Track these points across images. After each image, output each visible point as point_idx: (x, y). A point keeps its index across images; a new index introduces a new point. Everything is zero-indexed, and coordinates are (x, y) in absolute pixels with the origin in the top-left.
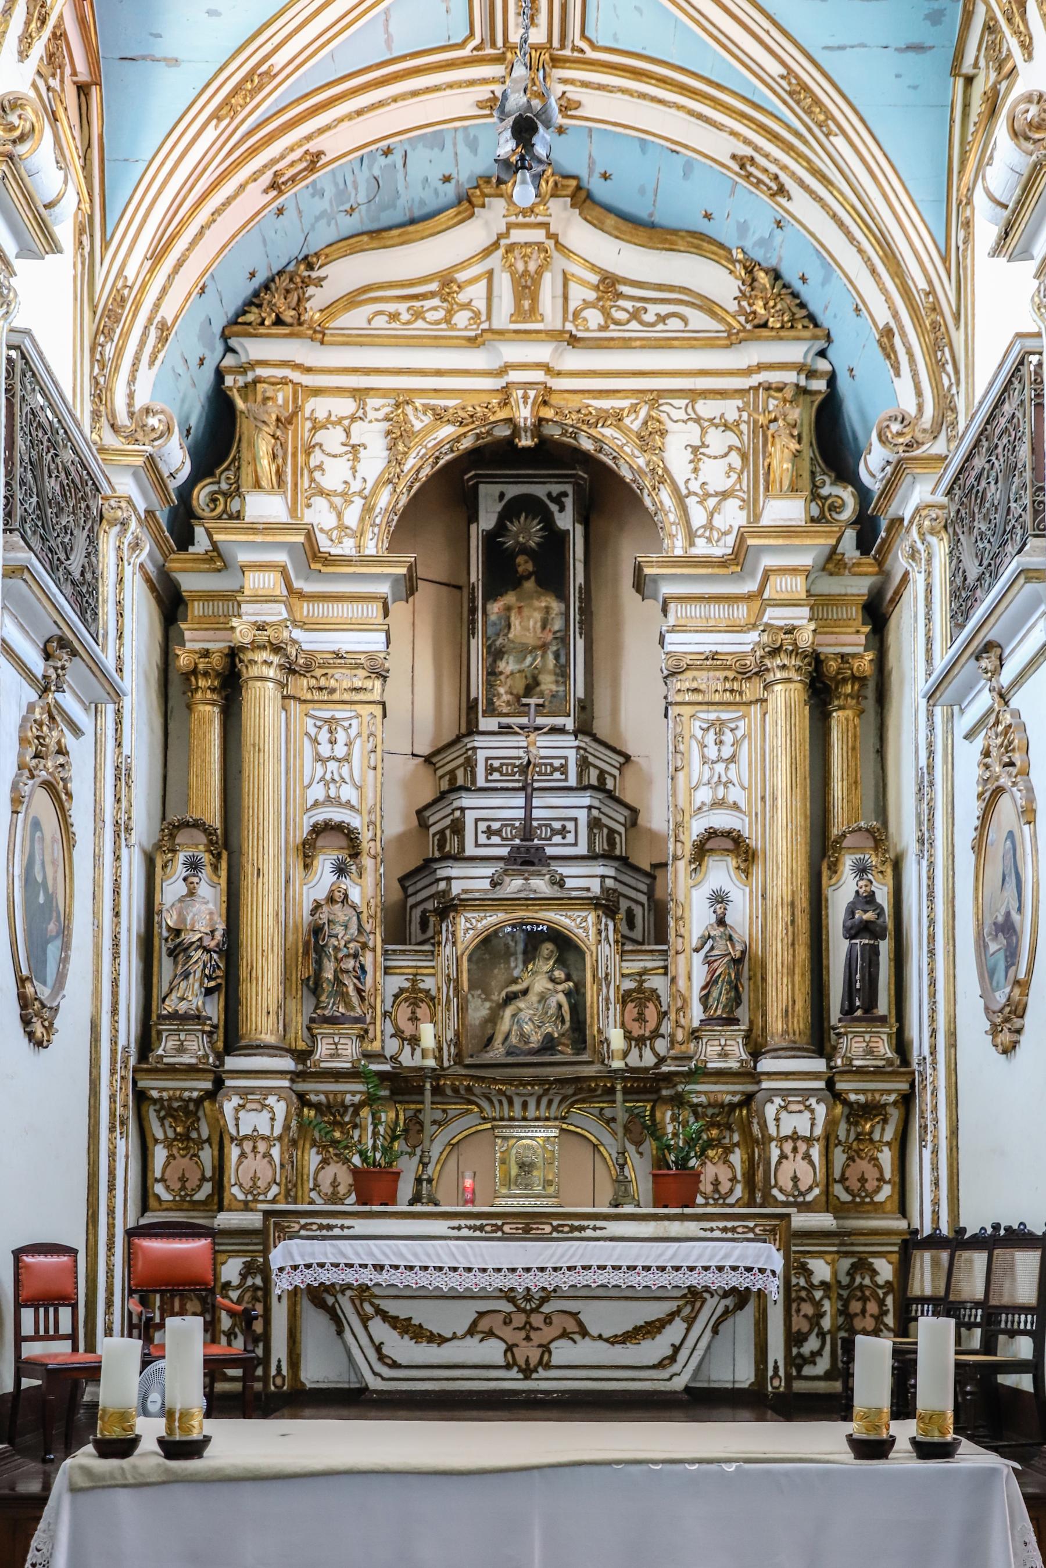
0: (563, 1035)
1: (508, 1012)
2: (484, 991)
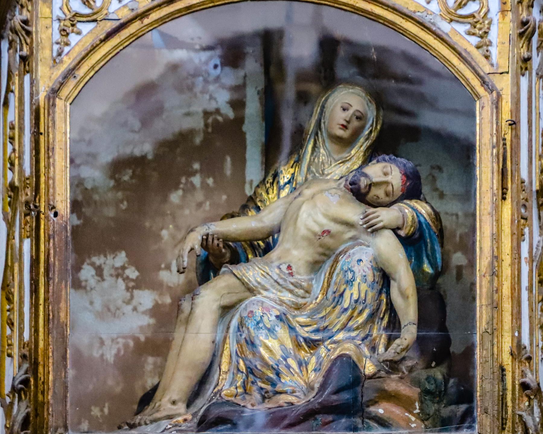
0: (393, 366)
1: (210, 297)
2: (135, 260)
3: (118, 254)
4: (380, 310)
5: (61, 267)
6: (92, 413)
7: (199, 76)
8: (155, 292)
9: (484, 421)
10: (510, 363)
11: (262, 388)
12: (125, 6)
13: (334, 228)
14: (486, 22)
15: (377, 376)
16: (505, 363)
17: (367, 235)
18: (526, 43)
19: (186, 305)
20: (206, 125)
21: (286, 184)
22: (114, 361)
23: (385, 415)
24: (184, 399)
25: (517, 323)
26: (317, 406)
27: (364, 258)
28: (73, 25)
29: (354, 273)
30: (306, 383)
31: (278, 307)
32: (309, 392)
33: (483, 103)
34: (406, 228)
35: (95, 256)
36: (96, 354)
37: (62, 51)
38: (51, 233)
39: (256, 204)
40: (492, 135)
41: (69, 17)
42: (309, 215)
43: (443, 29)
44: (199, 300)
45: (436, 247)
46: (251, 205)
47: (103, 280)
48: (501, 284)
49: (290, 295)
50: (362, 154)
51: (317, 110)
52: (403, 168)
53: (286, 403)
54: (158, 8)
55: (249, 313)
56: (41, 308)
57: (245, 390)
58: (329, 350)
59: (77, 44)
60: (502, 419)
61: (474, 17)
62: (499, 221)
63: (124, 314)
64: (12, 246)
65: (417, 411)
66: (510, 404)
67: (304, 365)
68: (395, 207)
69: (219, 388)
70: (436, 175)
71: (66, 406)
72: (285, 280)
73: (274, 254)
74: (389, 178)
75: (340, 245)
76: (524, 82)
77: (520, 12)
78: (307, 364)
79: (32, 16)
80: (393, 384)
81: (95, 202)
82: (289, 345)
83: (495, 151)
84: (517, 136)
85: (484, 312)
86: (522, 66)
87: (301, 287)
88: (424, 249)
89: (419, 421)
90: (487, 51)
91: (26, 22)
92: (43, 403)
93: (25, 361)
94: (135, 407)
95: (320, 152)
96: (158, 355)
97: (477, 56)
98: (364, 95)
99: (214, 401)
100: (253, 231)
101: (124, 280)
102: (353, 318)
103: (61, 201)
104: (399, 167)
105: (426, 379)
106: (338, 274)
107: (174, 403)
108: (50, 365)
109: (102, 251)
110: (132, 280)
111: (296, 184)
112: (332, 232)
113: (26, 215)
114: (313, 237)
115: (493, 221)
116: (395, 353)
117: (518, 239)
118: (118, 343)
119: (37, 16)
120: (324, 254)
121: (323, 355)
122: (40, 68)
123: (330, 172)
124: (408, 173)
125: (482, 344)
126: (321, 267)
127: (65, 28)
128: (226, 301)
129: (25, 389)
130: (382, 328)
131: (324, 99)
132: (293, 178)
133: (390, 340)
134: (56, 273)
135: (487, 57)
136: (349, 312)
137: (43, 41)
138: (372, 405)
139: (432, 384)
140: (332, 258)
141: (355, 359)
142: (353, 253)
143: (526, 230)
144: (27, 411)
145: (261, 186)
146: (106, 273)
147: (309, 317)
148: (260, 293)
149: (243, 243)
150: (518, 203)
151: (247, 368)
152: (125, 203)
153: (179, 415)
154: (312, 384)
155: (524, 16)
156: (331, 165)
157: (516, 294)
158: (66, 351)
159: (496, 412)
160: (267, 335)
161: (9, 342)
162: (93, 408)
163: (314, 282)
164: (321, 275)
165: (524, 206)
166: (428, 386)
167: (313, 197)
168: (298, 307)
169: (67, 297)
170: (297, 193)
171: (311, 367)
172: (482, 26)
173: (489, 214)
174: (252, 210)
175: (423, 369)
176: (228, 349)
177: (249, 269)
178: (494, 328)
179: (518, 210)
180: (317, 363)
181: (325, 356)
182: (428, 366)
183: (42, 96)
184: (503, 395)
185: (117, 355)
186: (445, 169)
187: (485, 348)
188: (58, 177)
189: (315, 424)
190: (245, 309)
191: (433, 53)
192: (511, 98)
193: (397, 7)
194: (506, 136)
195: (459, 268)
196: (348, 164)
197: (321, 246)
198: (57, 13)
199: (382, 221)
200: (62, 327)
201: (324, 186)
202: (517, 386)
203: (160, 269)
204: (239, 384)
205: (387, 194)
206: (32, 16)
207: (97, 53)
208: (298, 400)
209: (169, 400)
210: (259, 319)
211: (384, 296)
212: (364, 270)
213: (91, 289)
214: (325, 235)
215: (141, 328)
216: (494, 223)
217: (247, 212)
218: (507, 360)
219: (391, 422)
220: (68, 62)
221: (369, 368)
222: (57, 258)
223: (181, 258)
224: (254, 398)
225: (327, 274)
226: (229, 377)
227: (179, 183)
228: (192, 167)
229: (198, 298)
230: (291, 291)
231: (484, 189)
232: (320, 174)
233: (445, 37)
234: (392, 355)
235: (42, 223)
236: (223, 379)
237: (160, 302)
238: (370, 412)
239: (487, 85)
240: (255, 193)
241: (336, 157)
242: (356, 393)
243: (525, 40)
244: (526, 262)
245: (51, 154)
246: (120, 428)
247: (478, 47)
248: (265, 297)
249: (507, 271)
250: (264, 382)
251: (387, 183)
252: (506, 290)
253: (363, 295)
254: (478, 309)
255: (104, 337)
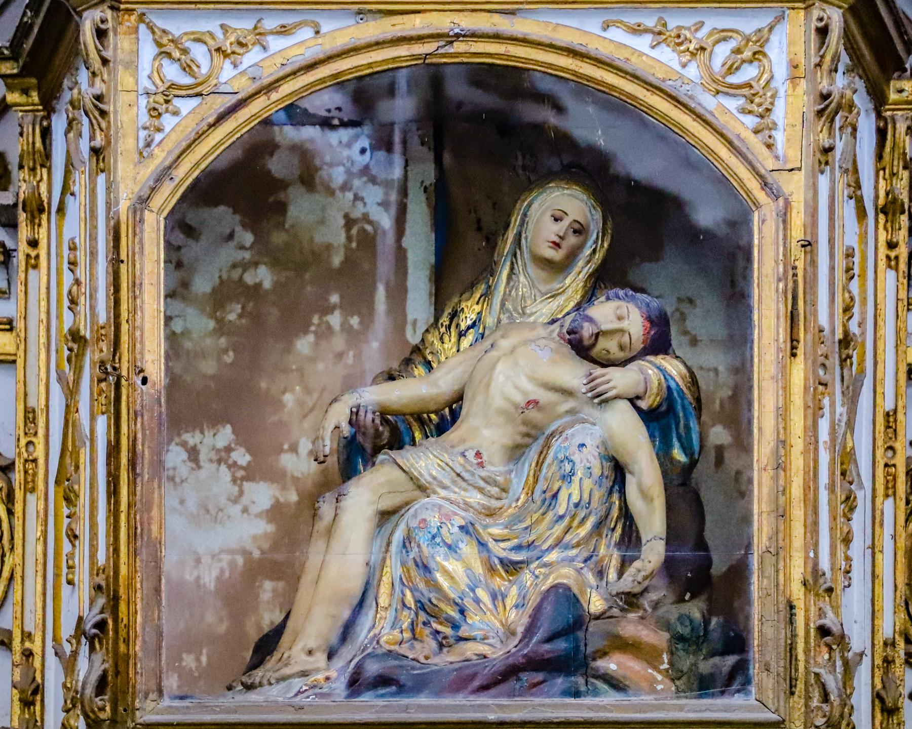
0: (630, 600)
2: (244, 437)
3: (221, 429)
4: (610, 517)
5: (152, 457)
6: (184, 664)
7: (338, 165)
8: (275, 485)
9: (764, 682)
10: (802, 597)
11: (438, 632)
12: (243, 73)
13: (545, 397)
14: (769, 94)
15: (608, 614)
16: (794, 597)
17: (593, 407)
18: (827, 125)
19: (326, 508)
20: (349, 238)
21: (469, 328)
22: (215, 587)
23: (619, 671)
24: (324, 647)
25: (812, 538)
26: (522, 660)
27: (588, 442)
28: (167, 102)
29: (574, 464)
30: (503, 625)
31: (463, 513)
32: (507, 638)
33: (765, 215)
34: (649, 397)
35: (187, 432)
36: (189, 577)
37: (152, 141)
38: (138, 408)
39: (425, 358)
40: (776, 262)
41: (161, 89)
42: (508, 378)
43: (705, 104)
44: (347, 503)
45: (691, 424)
46: (418, 359)
47: (199, 467)
48: (788, 482)
49: (479, 496)
50: (582, 284)
51: (516, 220)
52: (645, 309)
53: (476, 655)
54: (292, 77)
55: (420, 523)
56: (123, 517)
57: (414, 635)
58: (537, 577)
59: (173, 129)
60: (791, 679)
61: (751, 87)
62: (786, 389)
63: (229, 517)
64: (74, 422)
65: (666, 666)
66: (801, 656)
67: (500, 598)
68: (633, 366)
69: (376, 631)
70: (686, 311)
71: (160, 661)
72: (473, 474)
73: (452, 435)
74: (624, 325)
75: (552, 422)
76: (824, 181)
77: (819, 80)
78: (504, 597)
79: (108, 89)
80: (631, 627)
81: (188, 352)
82: (479, 569)
83: (781, 285)
84: (813, 263)
85: (765, 522)
86: (822, 160)
87: (496, 484)
88: (673, 426)
89: (667, 681)
90: (770, 137)
91: (99, 98)
92: (128, 655)
93: (100, 594)
94: (248, 655)
95: (519, 281)
96: (279, 579)
97: (755, 143)
98: (585, 198)
99: (369, 650)
100: (422, 400)
101: (229, 467)
102: (571, 530)
103: (153, 361)
104: (640, 308)
105: (679, 619)
106: (550, 466)
107: (310, 653)
108: (138, 600)
109: (196, 425)
110: (241, 468)
111: (484, 328)
112: (541, 402)
113: (100, 381)
114: (512, 410)
115: (779, 387)
116: (634, 581)
117: (814, 414)
118: (220, 560)
119: (116, 89)
120: (528, 435)
121: (529, 583)
122: (120, 165)
123: (534, 310)
124: (653, 317)
125: (761, 569)
126: (524, 453)
127: (157, 106)
128: (387, 503)
129: (101, 635)
130: (613, 543)
131: (526, 203)
132: (480, 320)
133: (624, 564)
134: (146, 466)
135: (769, 146)
136: (567, 520)
137: (124, 126)
138: (600, 657)
139: (686, 626)
140: (541, 441)
141: (575, 590)
142: (573, 435)
143: (826, 402)
144: (103, 667)
145: (432, 330)
146: (202, 457)
147: (506, 528)
148: (435, 492)
149: (408, 417)
150: (814, 362)
151: (418, 601)
152: (231, 354)
153: (317, 670)
154: (512, 627)
155: (824, 86)
156: (535, 300)
157: (811, 496)
158: (160, 580)
159: (782, 669)
160: (446, 555)
161: (70, 562)
162: (184, 656)
163: (513, 475)
164: (523, 464)
165: (824, 365)
166: (679, 629)
167: (513, 351)
168: (491, 513)
169: (161, 502)
170: (487, 344)
171: (509, 602)
172: (762, 100)
173: (772, 378)
174: (419, 367)
175: (673, 603)
176: (388, 574)
177: (420, 457)
178: (780, 546)
179: (815, 372)
180: (519, 595)
181: (532, 584)
182: (680, 600)
183: (124, 206)
184: (791, 644)
185: (218, 579)
186: (698, 302)
187: (767, 574)
188: (147, 326)
189: (517, 687)
190: (415, 516)
191: (691, 141)
192: (805, 208)
193: (639, 73)
194: (797, 263)
195: (720, 450)
196: (561, 300)
197: (525, 423)
198: (145, 83)
199: (614, 388)
200: (155, 546)
201: (528, 334)
202: (812, 630)
203: (281, 451)
204: (405, 626)
205: (622, 348)
206: (108, 89)
207: (203, 144)
208: (493, 650)
209: (303, 649)
210: (435, 531)
211: (615, 497)
212: (587, 460)
213: (182, 481)
214: (531, 406)
215: (254, 538)
216: (780, 392)
217: (412, 369)
218: (797, 592)
219: (627, 683)
220: (160, 157)
221: (596, 604)
222: (146, 446)
223: (321, 441)
224: (426, 646)
225: (534, 464)
226: (390, 615)
227: (310, 324)
228: (327, 300)
229: (345, 500)
230: (481, 490)
231: (765, 340)
232: (519, 313)
233: (709, 118)
234: (630, 585)
235: (124, 392)
236: (381, 618)
237: (282, 500)
238: (598, 668)
239: (771, 189)
240: (423, 340)
241: (543, 288)
242: (576, 640)
243: (825, 122)
244: (825, 448)
245: (137, 293)
246: (230, 688)
247: (756, 132)
248: (443, 498)
249: (797, 462)
250: (441, 623)
251: (622, 331)
252: (796, 490)
253: (586, 496)
254: (756, 517)
255: (201, 551)
